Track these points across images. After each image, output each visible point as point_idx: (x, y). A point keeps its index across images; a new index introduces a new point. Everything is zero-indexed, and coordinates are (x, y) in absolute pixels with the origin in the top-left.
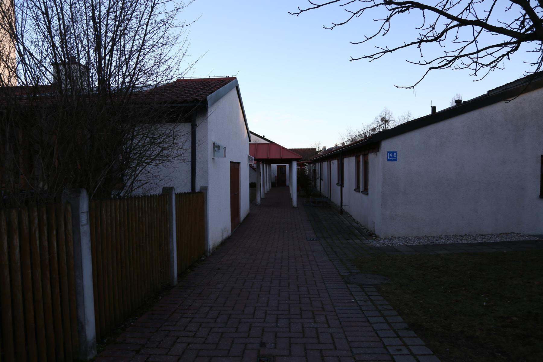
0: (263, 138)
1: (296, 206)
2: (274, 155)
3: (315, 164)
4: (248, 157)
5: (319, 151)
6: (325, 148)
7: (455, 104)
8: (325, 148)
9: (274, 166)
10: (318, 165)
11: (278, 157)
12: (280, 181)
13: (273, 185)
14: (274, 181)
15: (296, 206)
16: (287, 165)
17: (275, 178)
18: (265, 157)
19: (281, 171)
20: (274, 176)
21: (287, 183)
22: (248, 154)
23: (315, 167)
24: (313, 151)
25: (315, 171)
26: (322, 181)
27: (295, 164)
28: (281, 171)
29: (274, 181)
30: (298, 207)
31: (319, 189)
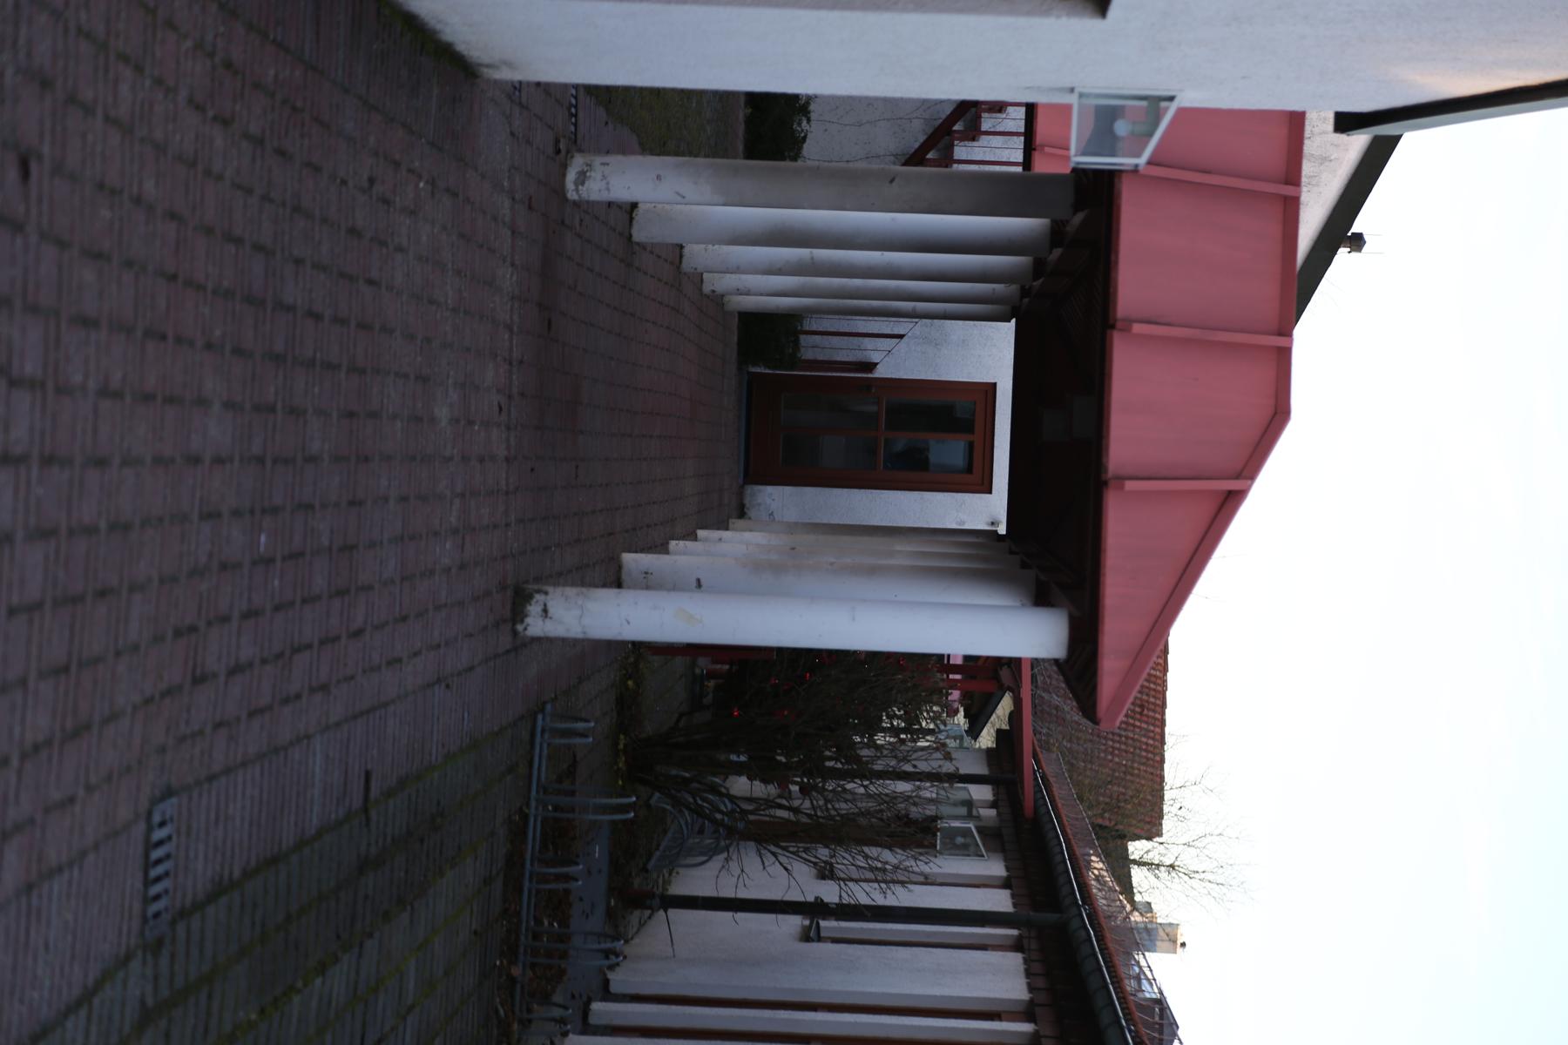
0: (1339, 232)
1: (535, 626)
2: (1146, 401)
3: (994, 839)
4: (1156, 103)
5: (1121, 867)
6: (1170, 938)
7: (1149, 993)
8: (1170, 938)
9: (987, 355)
10: (974, 881)
11: (1130, 437)
12: (803, 414)
13: (767, 335)
14: (811, 348)
15: (535, 626)
16: (988, 510)
17: (844, 351)
18: (1137, 283)
19: (919, 433)
20: (873, 350)
21: (781, 501)
22: (1191, 97)
23: (961, 846)
24: (1132, 800)
25: (918, 834)
26: (795, 922)
27: (1027, 634)
28: (919, 433)
29: (811, 348)
30: (523, 645)
31: (697, 880)
